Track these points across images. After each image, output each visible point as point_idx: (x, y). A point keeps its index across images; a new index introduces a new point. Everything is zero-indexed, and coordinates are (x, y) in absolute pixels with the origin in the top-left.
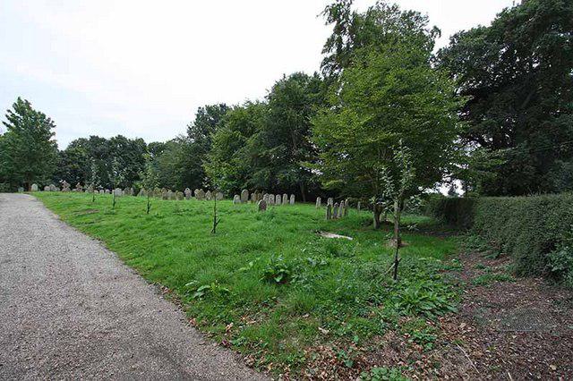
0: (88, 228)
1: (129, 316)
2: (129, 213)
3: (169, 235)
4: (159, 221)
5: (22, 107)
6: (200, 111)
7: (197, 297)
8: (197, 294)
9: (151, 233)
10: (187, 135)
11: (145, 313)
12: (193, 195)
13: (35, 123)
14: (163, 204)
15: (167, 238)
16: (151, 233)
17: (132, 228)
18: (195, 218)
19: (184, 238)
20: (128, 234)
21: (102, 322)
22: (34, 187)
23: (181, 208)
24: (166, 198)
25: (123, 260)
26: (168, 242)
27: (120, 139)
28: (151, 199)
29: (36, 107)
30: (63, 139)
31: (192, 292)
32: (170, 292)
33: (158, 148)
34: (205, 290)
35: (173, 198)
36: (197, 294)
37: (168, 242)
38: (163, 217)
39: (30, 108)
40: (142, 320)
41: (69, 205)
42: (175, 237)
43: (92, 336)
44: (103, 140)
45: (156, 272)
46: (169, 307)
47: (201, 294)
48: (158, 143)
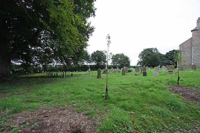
27: (167, 53)
44: (162, 54)
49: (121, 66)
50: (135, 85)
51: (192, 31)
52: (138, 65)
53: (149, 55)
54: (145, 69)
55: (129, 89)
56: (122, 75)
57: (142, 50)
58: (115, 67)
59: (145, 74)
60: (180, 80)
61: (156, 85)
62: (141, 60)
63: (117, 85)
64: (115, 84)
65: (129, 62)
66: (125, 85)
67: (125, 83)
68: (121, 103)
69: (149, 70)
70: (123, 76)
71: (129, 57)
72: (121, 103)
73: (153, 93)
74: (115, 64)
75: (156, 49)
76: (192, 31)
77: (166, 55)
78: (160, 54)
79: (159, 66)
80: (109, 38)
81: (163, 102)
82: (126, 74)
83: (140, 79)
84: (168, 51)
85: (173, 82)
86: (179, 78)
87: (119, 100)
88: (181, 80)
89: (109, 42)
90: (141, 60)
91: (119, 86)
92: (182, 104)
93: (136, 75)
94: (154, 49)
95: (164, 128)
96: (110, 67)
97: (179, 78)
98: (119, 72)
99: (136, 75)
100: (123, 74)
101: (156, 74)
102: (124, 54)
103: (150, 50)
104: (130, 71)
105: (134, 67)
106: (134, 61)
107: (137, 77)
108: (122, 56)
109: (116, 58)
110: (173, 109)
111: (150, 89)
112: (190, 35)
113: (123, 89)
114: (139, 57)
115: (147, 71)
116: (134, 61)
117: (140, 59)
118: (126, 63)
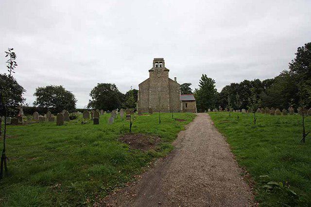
0: (222, 129)
1: (219, 182)
2: (164, 131)
3: (263, 139)
4: (260, 129)
5: (204, 78)
6: (300, 50)
7: (266, 188)
8: (266, 186)
9: (252, 136)
10: (289, 70)
11: (228, 184)
12: (296, 111)
13: (208, 83)
14: (263, 117)
15: (262, 141)
16: (252, 136)
17: (241, 132)
18: (290, 129)
19: (274, 143)
20: (239, 135)
21: (206, 179)
22: (209, 110)
23: (281, 121)
24: (273, 114)
25: (231, 149)
26: (260, 144)
27: (246, 82)
28: (256, 114)
29: (208, 77)
30: (219, 88)
31: (263, 183)
32: (249, 177)
33: (269, 83)
34: (274, 185)
35: (279, 114)
36: (266, 186)
37: (260, 144)
38: (264, 126)
39: (206, 77)
40: (225, 187)
41: (219, 118)
42: (267, 141)
43: (199, 185)
44: (237, 84)
45: (246, 161)
46: (244, 187)
47: (270, 187)
48: (268, 80)
49: (57, 108)
50: (74, 140)
51: (149, 71)
52: (88, 107)
53: (105, 93)
54: (97, 115)
55: (61, 148)
56: (57, 125)
57: (96, 85)
58: (42, 111)
59: (96, 122)
60: (132, 126)
61: (107, 137)
62: (95, 99)
63: (38, 145)
64: (37, 143)
65: (73, 103)
66: (57, 142)
67: (58, 139)
68: (37, 177)
69: (104, 116)
70: (58, 127)
71: (73, 93)
72: (37, 177)
73: (97, 148)
74: (44, 105)
75: (114, 86)
76: (149, 71)
77: (126, 95)
78: (120, 94)
79: (117, 109)
80: (13, 56)
81: (106, 157)
82: (65, 122)
83: (89, 130)
84: (251, 79)
85: (126, 129)
86: (131, 125)
87: (34, 172)
88: (135, 127)
89: (14, 63)
90: (95, 99)
91: (43, 146)
92: (126, 154)
93: (82, 123)
94: (112, 85)
95: (100, 189)
96: (29, 111)
97: (131, 125)
98: (51, 120)
99: (82, 123)
100: (60, 123)
101: (111, 121)
102: (63, 87)
103: (107, 86)
104: (75, 118)
105: (82, 111)
106: (83, 101)
107: (82, 127)
108: (60, 90)
109: (44, 94)
110: (117, 163)
111: (96, 143)
112: (147, 76)
113: (50, 149)
114: (91, 95)
115: (101, 116)
116: (83, 101)
117: (93, 98)
118: (67, 103)
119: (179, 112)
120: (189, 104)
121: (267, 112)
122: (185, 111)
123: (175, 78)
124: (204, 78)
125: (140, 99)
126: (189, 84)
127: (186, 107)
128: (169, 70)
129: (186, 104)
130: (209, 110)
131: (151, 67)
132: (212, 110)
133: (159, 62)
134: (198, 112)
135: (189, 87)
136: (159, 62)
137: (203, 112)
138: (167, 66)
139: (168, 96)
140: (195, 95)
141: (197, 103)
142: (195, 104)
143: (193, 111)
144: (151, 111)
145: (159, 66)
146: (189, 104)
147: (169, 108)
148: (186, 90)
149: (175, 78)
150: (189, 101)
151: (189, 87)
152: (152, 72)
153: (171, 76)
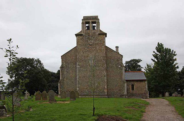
5: (160, 48)
22: (167, 94)
29: (165, 46)
75: (39, 61)
76: (76, 35)
78: (46, 72)
112: (72, 43)
119: (122, 96)
120: (136, 84)
121: (45, 98)
122: (130, 95)
123: (117, 47)
124: (160, 48)
125: (63, 78)
126: (139, 61)
127: (133, 89)
128: (105, 34)
129: (133, 86)
130: (167, 94)
131: (79, 29)
132: (170, 95)
133: (141, 61)
134: (151, 96)
135: (139, 64)
136: (90, 21)
137: (157, 96)
138: (103, 28)
139: (105, 73)
140: (146, 74)
141: (149, 83)
142: (145, 85)
143: (143, 96)
144: (73, 95)
145: (91, 28)
146: (136, 84)
147: (106, 91)
148: (134, 67)
149: (117, 47)
150: (137, 81)
151: (139, 64)
152: (81, 37)
153: (110, 43)
